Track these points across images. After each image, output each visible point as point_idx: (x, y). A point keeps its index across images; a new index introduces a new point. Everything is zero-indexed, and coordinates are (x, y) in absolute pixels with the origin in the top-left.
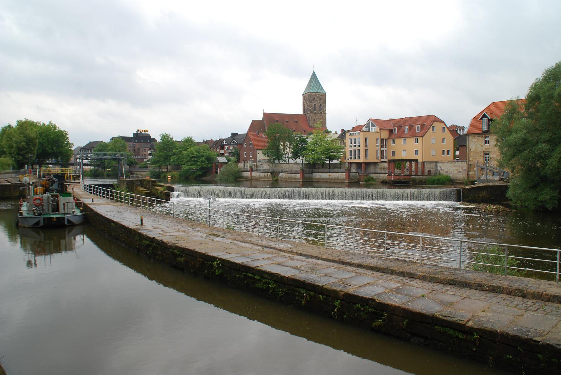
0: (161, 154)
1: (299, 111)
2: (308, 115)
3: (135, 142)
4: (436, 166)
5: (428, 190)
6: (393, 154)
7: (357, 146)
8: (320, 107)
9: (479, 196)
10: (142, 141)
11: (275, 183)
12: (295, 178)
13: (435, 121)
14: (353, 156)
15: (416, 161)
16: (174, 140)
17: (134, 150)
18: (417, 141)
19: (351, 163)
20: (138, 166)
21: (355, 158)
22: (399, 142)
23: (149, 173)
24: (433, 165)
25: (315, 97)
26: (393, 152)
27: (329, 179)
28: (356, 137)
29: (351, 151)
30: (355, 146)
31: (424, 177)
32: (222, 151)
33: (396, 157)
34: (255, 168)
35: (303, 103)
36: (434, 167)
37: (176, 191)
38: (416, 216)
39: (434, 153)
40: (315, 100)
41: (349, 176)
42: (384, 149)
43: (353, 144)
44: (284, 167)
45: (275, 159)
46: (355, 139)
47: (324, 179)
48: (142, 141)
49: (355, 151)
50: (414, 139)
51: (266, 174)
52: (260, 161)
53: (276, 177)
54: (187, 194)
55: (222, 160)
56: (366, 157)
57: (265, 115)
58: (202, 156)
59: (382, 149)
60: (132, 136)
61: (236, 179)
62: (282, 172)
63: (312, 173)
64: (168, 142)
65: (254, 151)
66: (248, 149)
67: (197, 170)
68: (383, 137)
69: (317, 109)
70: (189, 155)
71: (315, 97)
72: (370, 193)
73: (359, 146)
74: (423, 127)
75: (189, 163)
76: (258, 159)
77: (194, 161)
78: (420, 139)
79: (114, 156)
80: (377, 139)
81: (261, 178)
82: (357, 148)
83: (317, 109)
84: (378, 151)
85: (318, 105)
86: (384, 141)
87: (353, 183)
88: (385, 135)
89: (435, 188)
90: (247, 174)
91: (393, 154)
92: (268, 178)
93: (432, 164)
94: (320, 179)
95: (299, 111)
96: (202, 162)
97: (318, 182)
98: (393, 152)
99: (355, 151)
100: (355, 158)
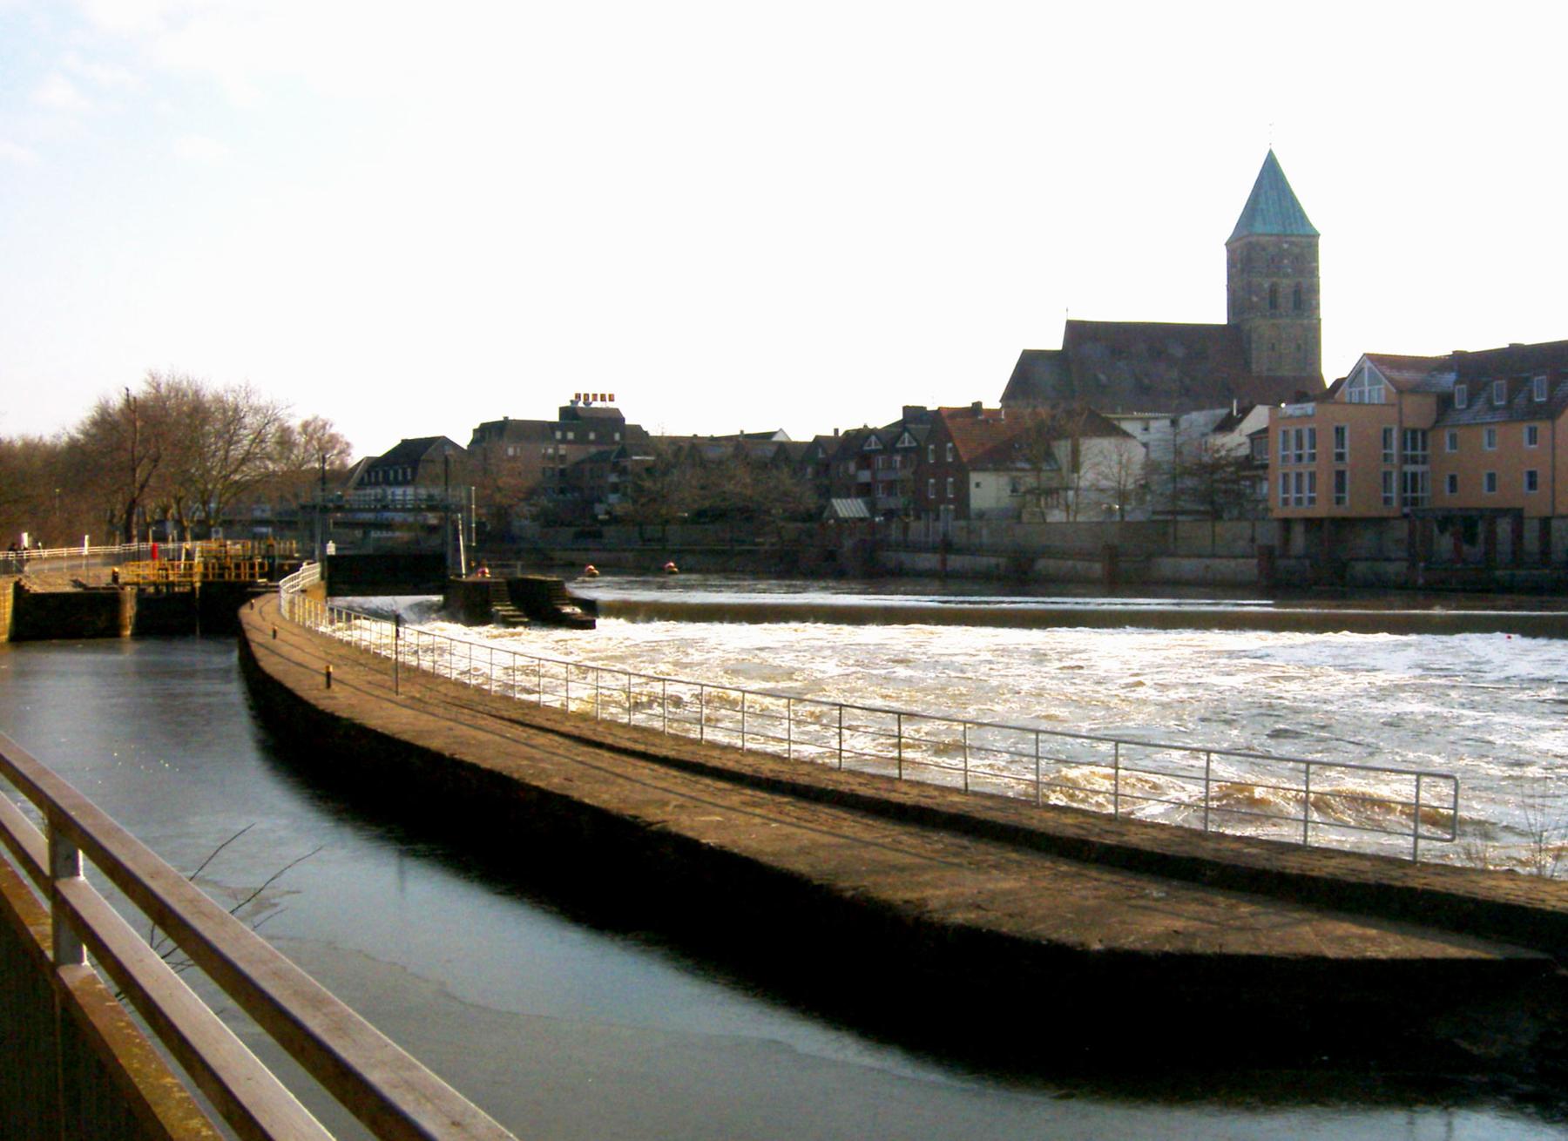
1: (1211, 309)
3: (564, 440)
15: (1518, 516)
26: (1453, 479)
29: (1286, 476)
30: (1300, 458)
38: (661, 571)
49: (1299, 476)
51: (993, 561)
56: (1339, 501)
59: (1410, 468)
60: (554, 417)
82: (1306, 468)
84: (1386, 476)
86: (1413, 437)
91: (1492, 487)
95: (1211, 309)
99: (1299, 476)
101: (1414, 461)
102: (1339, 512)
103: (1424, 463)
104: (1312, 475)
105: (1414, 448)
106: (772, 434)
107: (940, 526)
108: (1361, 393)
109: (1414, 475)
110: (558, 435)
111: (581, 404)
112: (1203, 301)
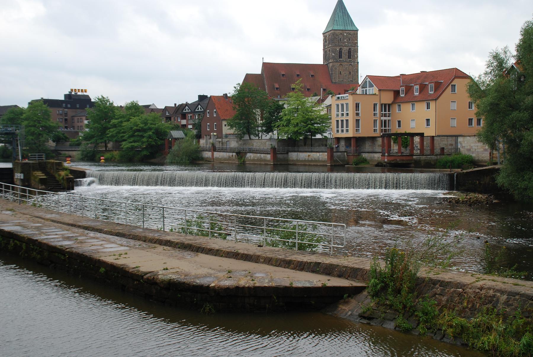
0: (96, 125)
2: (331, 65)
3: (66, 107)
4: (456, 143)
5: (409, 175)
6: (399, 126)
7: (345, 115)
8: (349, 52)
9: (480, 183)
10: (78, 106)
11: (243, 167)
12: (265, 160)
13: (456, 77)
14: (340, 129)
15: (421, 135)
16: (115, 105)
17: (66, 120)
18: (428, 107)
19: (338, 139)
20: (68, 144)
21: (342, 131)
22: (407, 108)
23: (79, 152)
24: (451, 141)
25: (341, 36)
26: (399, 122)
27: (308, 161)
28: (344, 102)
29: (338, 121)
30: (343, 115)
31: (434, 157)
32: (184, 122)
33: (402, 130)
34: (217, 146)
35: (324, 46)
36: (454, 143)
37: (89, 177)
39: (454, 123)
40: (342, 41)
41: (331, 157)
42: (387, 118)
43: (340, 112)
44: (255, 144)
45: (244, 133)
46: (342, 105)
47: (302, 161)
48: (78, 106)
49: (342, 121)
50: (425, 105)
51: (231, 154)
52: (227, 136)
53: (243, 158)
54: (102, 181)
55: (176, 134)
57: (266, 66)
58: (150, 129)
59: (383, 118)
60: (62, 98)
61: (194, 160)
62: (251, 151)
63: (287, 153)
64: (105, 108)
65: (219, 120)
66: (212, 120)
67: (143, 149)
68: (384, 101)
69: (345, 56)
70: (131, 128)
71: (341, 36)
72: (384, 180)
73: (347, 114)
74: (438, 86)
75: (132, 139)
76: (224, 133)
77: (138, 136)
78: (432, 104)
79: (6, 130)
80: (375, 105)
81: (225, 159)
82: (344, 118)
83: (345, 56)
84: (375, 121)
85: (345, 50)
86: (386, 107)
87: (336, 165)
88: (388, 98)
89: (422, 172)
90: (207, 155)
91: (399, 126)
92: (234, 160)
93: (450, 139)
94: (297, 160)
96: (150, 137)
97: (295, 165)
98: (399, 122)
99: (342, 121)
100: (342, 131)
101: (385, 116)
102: (358, 135)
103: (389, 116)
104: (347, 121)
105: (385, 111)
106: (149, 106)
107: (211, 141)
108: (366, 90)
109: (385, 121)
110: (64, 105)
111: (73, 93)
112: (313, 54)
